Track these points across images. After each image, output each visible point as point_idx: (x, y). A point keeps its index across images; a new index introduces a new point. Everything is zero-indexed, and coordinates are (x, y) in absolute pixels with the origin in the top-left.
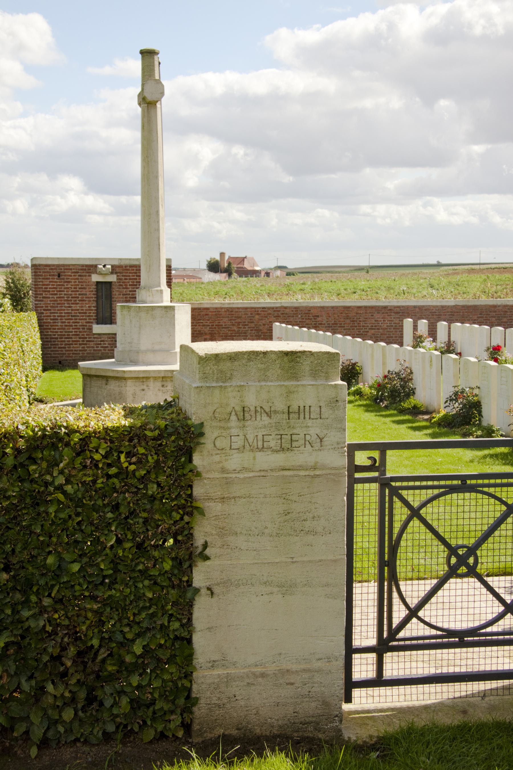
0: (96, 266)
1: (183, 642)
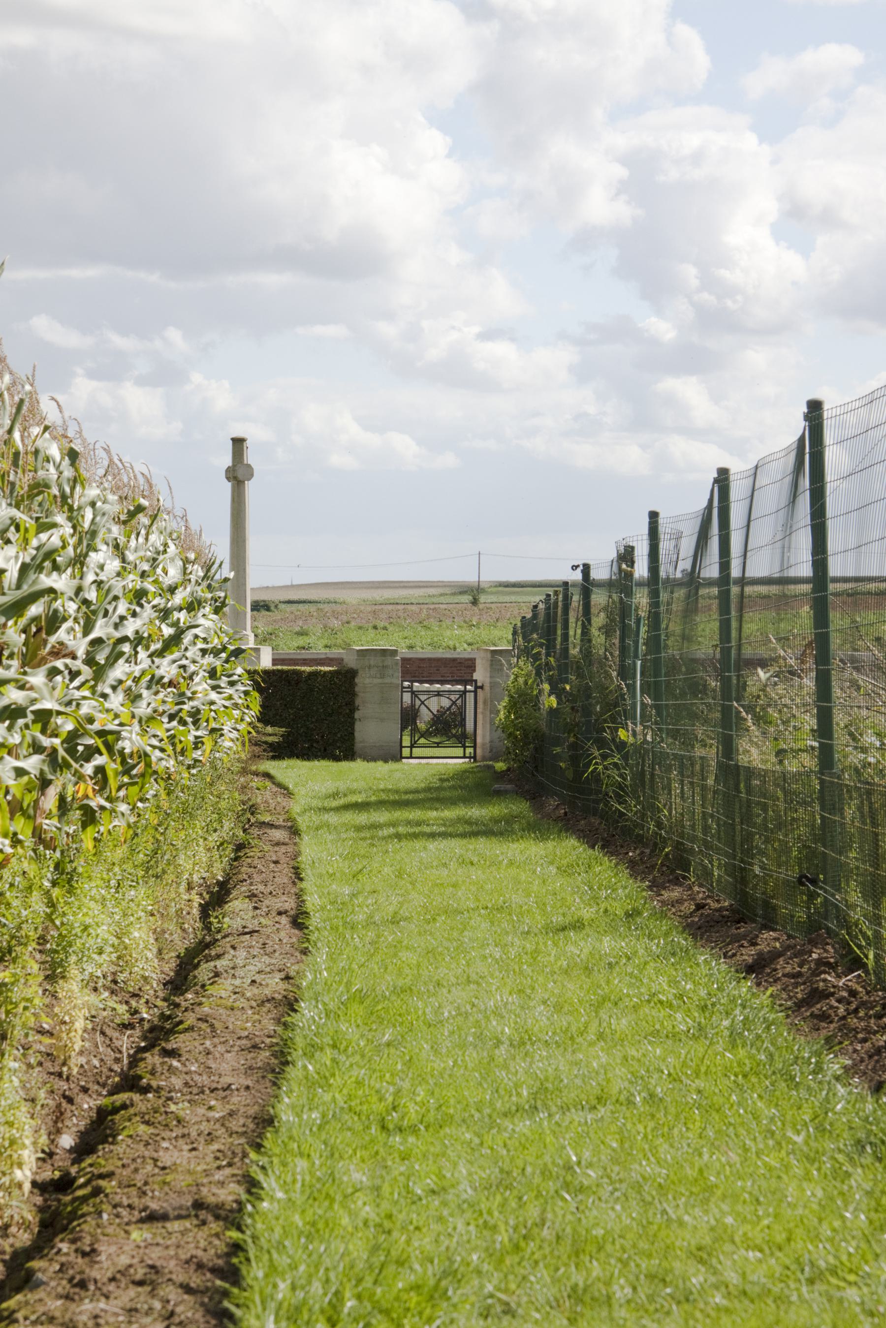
1: (352, 734)
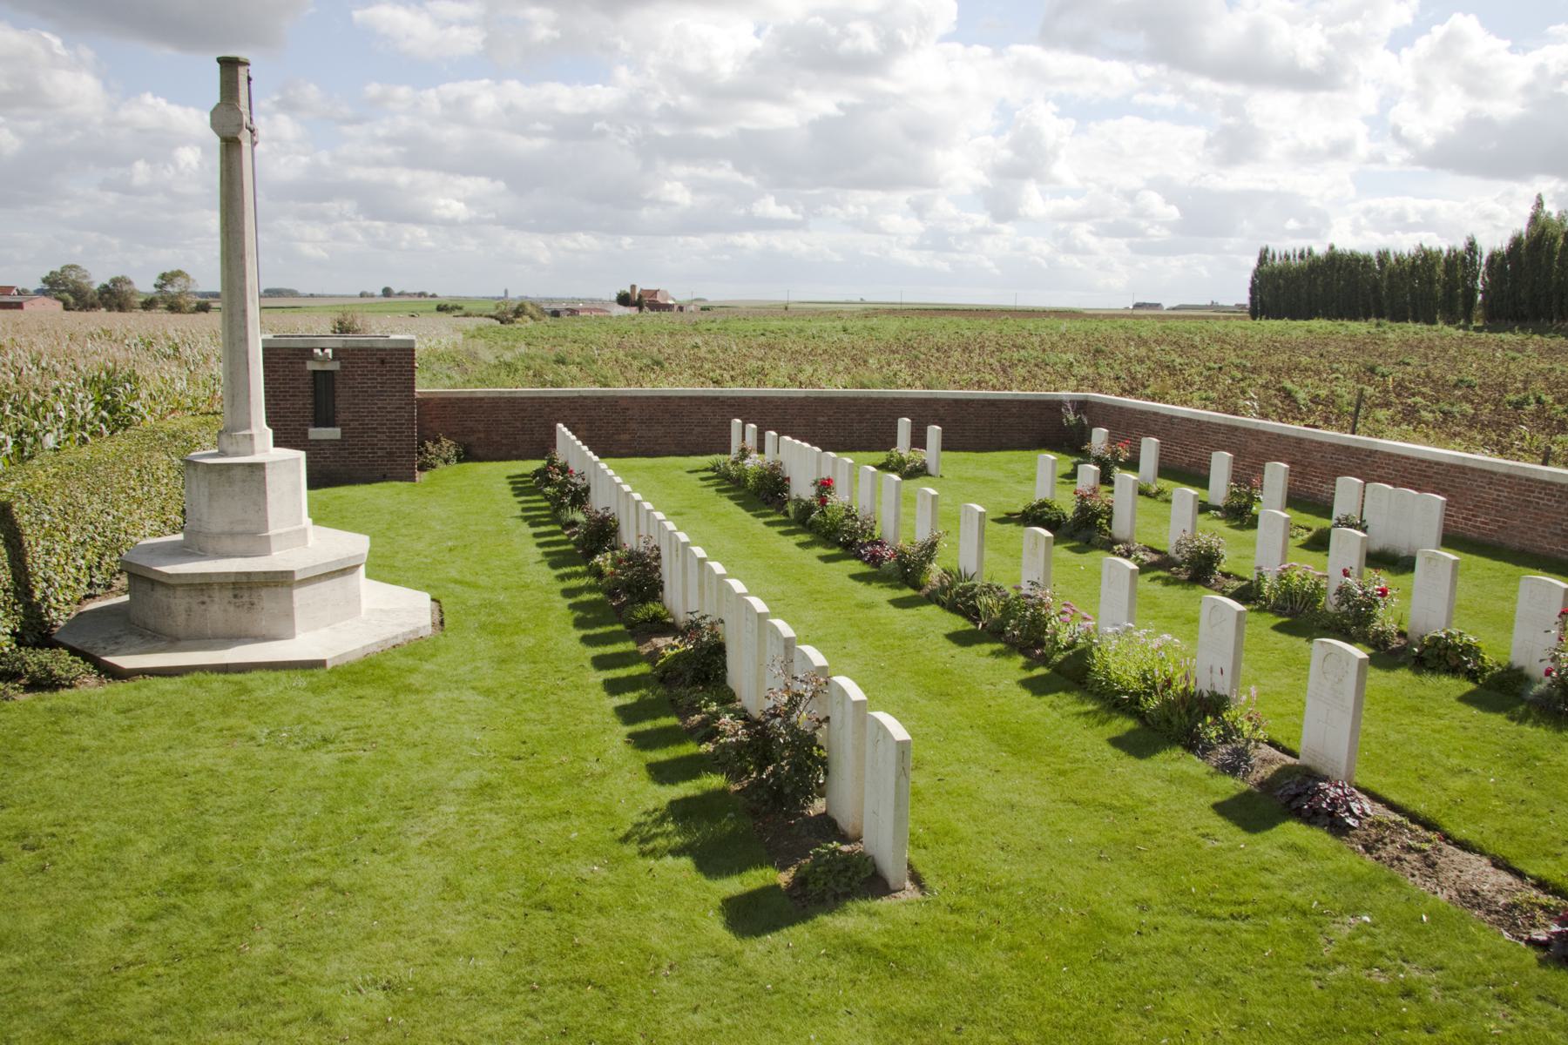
0: (311, 350)
